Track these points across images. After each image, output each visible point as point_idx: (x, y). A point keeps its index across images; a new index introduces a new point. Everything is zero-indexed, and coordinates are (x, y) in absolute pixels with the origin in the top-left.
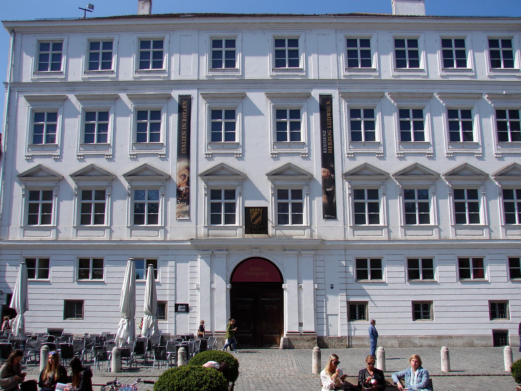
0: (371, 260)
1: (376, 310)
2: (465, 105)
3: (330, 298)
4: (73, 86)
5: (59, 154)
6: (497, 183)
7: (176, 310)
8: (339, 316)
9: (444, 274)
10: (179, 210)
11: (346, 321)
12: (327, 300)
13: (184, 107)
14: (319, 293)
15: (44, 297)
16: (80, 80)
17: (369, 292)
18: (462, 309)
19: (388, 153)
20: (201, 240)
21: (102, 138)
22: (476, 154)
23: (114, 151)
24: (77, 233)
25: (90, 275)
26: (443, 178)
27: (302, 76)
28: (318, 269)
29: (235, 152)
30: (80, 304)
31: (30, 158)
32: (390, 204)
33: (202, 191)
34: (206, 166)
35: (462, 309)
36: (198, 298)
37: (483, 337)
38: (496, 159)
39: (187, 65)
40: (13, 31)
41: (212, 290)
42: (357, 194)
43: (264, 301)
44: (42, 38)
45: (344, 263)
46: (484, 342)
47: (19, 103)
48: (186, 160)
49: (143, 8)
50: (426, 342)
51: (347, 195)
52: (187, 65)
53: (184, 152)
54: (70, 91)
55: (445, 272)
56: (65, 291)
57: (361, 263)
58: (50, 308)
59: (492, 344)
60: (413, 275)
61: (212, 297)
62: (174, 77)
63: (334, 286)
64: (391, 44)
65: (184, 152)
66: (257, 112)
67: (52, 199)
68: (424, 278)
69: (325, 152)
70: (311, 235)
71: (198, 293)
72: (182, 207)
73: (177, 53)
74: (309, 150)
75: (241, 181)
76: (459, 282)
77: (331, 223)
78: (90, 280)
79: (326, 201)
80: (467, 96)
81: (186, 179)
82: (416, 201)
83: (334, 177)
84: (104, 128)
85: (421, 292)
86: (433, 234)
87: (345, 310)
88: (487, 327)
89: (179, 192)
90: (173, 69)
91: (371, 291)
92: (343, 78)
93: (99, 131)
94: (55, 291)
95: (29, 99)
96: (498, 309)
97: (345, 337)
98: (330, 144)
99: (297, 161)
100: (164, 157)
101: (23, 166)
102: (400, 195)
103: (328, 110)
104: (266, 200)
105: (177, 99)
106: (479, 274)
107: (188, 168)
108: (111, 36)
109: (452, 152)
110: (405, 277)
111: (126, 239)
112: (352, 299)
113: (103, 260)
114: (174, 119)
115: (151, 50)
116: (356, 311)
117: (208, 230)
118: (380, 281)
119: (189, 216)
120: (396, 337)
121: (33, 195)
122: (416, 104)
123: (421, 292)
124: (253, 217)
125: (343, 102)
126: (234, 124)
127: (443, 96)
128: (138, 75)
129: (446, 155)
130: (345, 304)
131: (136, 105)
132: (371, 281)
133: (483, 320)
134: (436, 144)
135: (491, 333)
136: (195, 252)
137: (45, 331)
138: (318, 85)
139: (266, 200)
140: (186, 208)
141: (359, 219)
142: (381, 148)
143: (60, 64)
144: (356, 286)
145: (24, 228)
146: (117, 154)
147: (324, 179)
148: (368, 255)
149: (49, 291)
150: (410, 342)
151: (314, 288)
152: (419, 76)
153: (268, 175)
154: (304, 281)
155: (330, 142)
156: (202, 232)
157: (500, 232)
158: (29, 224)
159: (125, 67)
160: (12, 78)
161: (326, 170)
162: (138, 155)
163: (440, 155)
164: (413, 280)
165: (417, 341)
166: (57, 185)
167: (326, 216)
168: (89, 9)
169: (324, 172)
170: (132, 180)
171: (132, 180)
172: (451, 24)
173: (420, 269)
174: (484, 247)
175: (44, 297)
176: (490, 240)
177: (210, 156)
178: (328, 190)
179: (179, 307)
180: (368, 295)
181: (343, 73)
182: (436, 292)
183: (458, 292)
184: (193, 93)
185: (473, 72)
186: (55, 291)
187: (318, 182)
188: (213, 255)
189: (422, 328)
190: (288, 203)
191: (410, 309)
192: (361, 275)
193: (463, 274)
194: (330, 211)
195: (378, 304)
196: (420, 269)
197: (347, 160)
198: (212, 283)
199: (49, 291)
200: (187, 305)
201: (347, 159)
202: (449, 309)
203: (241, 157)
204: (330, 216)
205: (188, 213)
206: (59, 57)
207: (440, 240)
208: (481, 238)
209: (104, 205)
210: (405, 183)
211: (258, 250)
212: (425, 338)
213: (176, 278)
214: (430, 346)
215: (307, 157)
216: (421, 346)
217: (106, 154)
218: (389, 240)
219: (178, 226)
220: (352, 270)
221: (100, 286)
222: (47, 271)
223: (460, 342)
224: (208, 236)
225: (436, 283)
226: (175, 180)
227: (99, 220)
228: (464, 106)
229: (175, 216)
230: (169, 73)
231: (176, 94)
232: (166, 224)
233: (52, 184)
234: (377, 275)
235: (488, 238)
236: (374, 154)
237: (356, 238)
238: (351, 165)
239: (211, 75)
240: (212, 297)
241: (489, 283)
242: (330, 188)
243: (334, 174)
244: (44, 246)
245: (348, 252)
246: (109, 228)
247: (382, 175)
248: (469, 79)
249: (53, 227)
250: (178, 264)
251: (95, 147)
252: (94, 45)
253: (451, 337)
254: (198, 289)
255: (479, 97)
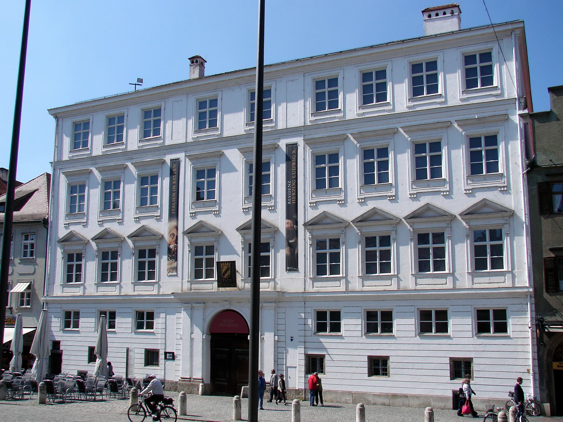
0: (331, 312)
1: (332, 364)
2: (432, 136)
3: (291, 350)
4: (94, 159)
5: (448, 189)
6: (464, 224)
7: (166, 358)
8: (297, 368)
9: (402, 328)
10: (170, 266)
11: (303, 374)
12: (287, 352)
13: (174, 170)
14: (280, 344)
15: (76, 343)
16: (101, 154)
17: (326, 345)
18: (420, 366)
19: (349, 200)
20: (185, 294)
21: (384, 178)
22: (442, 192)
23: (346, 196)
24: (473, 280)
25: (492, 329)
26: (459, 218)
27: (272, 127)
28: (280, 322)
29: (213, 209)
30: (468, 363)
31: (315, 205)
32: (349, 253)
33: (187, 249)
34: (190, 223)
35: (420, 366)
36: (181, 347)
37: (441, 399)
38: (465, 196)
39: (178, 129)
40: (56, 117)
41: (192, 339)
42: (320, 244)
43: (238, 351)
44: (76, 119)
45: (303, 315)
46: (442, 404)
47: (61, 179)
48: (175, 220)
49: (194, 72)
50: (380, 400)
51: (309, 246)
52: (178, 129)
53: (174, 214)
54: (93, 165)
55: (405, 325)
56: (89, 339)
57: (321, 315)
58: (79, 353)
59: (451, 406)
60: (371, 329)
61: (191, 347)
62: (168, 142)
63: (294, 339)
64: (460, 61)
65: (174, 214)
66: (233, 169)
67: (389, 245)
68: (382, 331)
69: (289, 203)
70: (275, 288)
71: (181, 342)
72: (171, 264)
73: (170, 120)
74: (276, 202)
75: (344, 229)
76: (418, 337)
77: (293, 275)
78: (327, 333)
79: (289, 253)
80: (431, 127)
81: (175, 238)
82: (488, 243)
83: (297, 228)
84: (384, 165)
85: (377, 347)
86: (446, 283)
87: (303, 362)
88: (447, 387)
89: (169, 250)
90: (167, 135)
91: (329, 344)
92: (309, 124)
93: (330, 175)
94: (83, 339)
95: (67, 175)
96: (461, 368)
97: (302, 390)
98: (294, 194)
99: (494, 197)
100: (159, 218)
101: (62, 233)
102: (359, 243)
103: (294, 159)
104: (238, 255)
105: (284, 148)
106: (443, 328)
107: (177, 228)
108: (122, 111)
109: (415, 192)
110: (362, 331)
111: (59, 295)
112: (310, 352)
113: (340, 312)
114: (166, 182)
115: (424, 74)
116: (315, 364)
117: (191, 284)
118: (445, 334)
119: (177, 272)
120: (350, 393)
121: (70, 257)
122: (379, 142)
123: (377, 347)
124: (224, 270)
125: (308, 148)
126: (440, 157)
127: (463, 123)
128: (141, 144)
129: (410, 196)
130: (303, 357)
131: (140, 172)
132: (494, 335)
133: (442, 380)
134: (400, 184)
135: (450, 394)
136: (179, 305)
137: (76, 373)
138: (286, 134)
139: (238, 255)
140: (174, 265)
141: (320, 271)
142: (448, 186)
143: (337, 101)
144: (314, 338)
145: (63, 286)
146: (125, 218)
147: (288, 231)
148: (328, 307)
149: (79, 339)
150: (364, 399)
151: (275, 341)
152: (384, 111)
153: (238, 230)
154: (266, 333)
155: (294, 192)
156: (186, 286)
157: (356, 284)
158: (102, 281)
159: (133, 138)
160: (56, 158)
161: (290, 221)
162: (196, 213)
163: (457, 191)
164: (371, 334)
165: (370, 399)
166: (508, 222)
167: (288, 268)
168: (138, 83)
169: (288, 223)
170: (312, 230)
171: (312, 230)
172: (420, 46)
173: (379, 322)
174: (447, 298)
175: (76, 343)
176: (514, 287)
177: (415, 196)
178: (290, 241)
179: (168, 354)
180: (325, 349)
181: (310, 119)
182: (393, 347)
183: (416, 347)
184: (299, 141)
185: (443, 97)
186: (83, 339)
187: (519, 218)
188: (192, 308)
189: (378, 385)
190: (326, 253)
191: (366, 364)
192: (321, 328)
193: (424, 328)
194: (292, 264)
195: (335, 358)
196: (379, 322)
197: (309, 209)
198: (192, 333)
199: (79, 339)
200: (173, 353)
201: (309, 208)
202: (406, 366)
203: (218, 214)
204: (292, 268)
205: (176, 269)
206: (434, 78)
207: (158, 295)
208: (444, 287)
209: (501, 246)
210: (416, 226)
211: (227, 302)
212: (379, 396)
213: (166, 329)
214: (384, 404)
215: (506, 190)
216: (375, 404)
217: (118, 218)
218: (454, 289)
219: (174, 279)
220: (311, 322)
221: (152, 337)
222: (339, 324)
223: (416, 402)
224: (191, 290)
225: (449, 337)
226: (167, 239)
227: (386, 268)
228: (432, 138)
229: (166, 272)
230: (276, 123)
231: (168, 158)
232: (513, 268)
233: (154, 243)
234: (336, 328)
235: (451, 286)
236: (153, 217)
237: (315, 289)
238: (312, 214)
239: (362, 112)
240: (191, 347)
241: (511, 338)
242: (292, 239)
243: (297, 225)
244: (74, 300)
245: (307, 304)
246: (397, 276)
247: (505, 211)
248: (438, 106)
249: (393, 276)
250: (168, 316)
251: (376, 189)
252: (416, 68)
253: (406, 396)
254: (181, 339)
255: (449, 125)
